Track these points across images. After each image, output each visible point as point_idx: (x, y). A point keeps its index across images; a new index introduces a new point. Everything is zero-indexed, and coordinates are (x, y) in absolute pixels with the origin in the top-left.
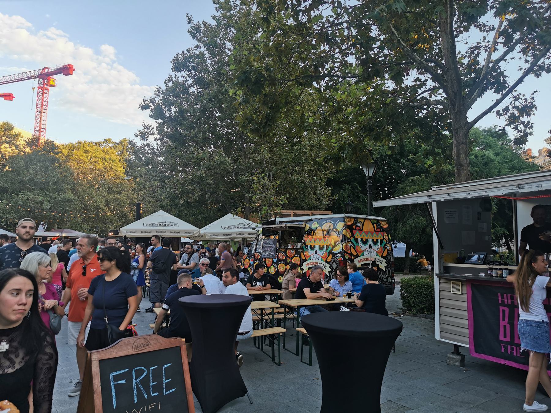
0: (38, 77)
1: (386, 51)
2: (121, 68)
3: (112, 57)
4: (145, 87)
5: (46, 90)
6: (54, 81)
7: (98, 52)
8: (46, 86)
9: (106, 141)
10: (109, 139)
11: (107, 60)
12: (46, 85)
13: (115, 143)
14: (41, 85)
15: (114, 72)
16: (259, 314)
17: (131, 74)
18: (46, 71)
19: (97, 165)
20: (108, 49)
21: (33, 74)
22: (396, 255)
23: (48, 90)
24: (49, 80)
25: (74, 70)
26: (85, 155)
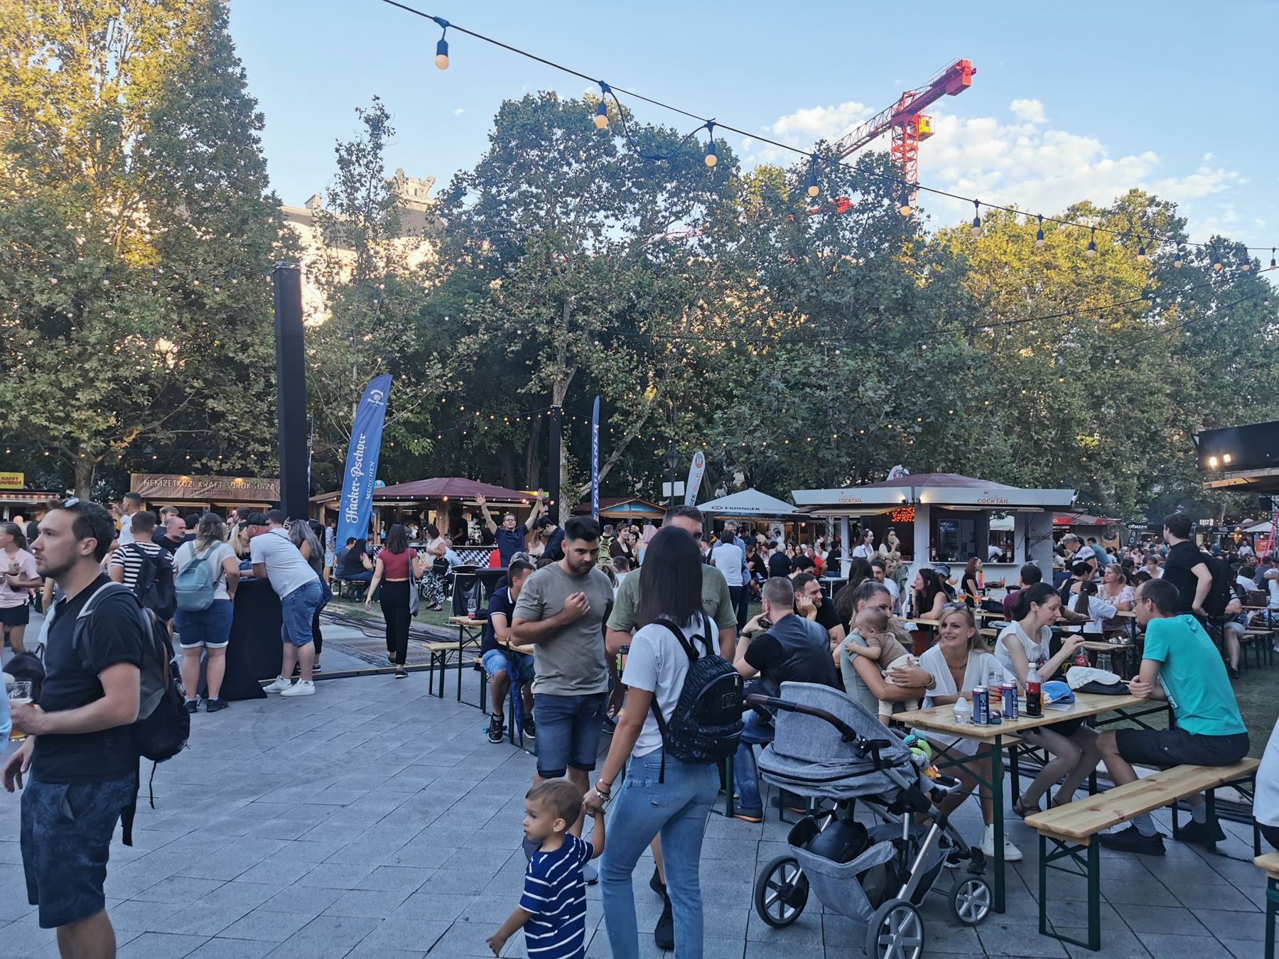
0: (890, 125)
1: (1043, 462)
2: (1062, 135)
3: (1040, 119)
4: (1124, 161)
5: (912, 150)
6: (927, 124)
7: (1007, 119)
8: (909, 142)
9: (1074, 211)
10: (1086, 203)
11: (1029, 128)
12: (911, 137)
13: (1104, 213)
14: (900, 142)
15: (1045, 150)
16: (974, 578)
17: (1086, 141)
18: (908, 101)
19: (1052, 273)
20: (1031, 108)
21: (881, 120)
22: (275, 497)
23: (913, 149)
24: (914, 124)
25: (974, 72)
26: (1011, 248)
